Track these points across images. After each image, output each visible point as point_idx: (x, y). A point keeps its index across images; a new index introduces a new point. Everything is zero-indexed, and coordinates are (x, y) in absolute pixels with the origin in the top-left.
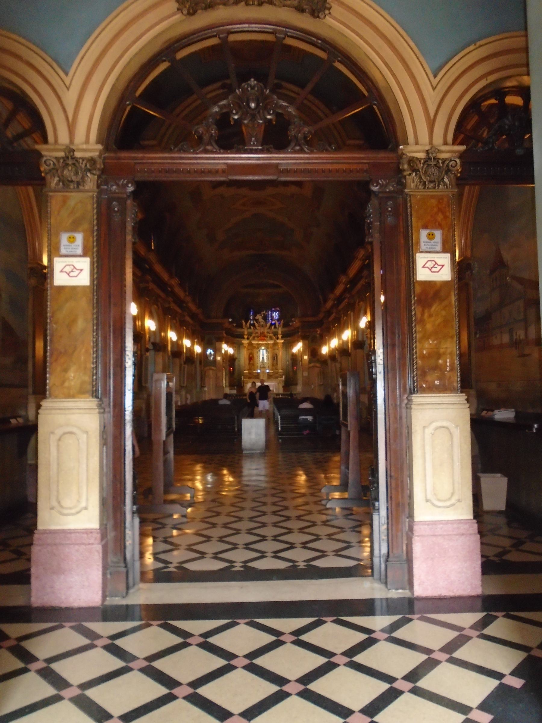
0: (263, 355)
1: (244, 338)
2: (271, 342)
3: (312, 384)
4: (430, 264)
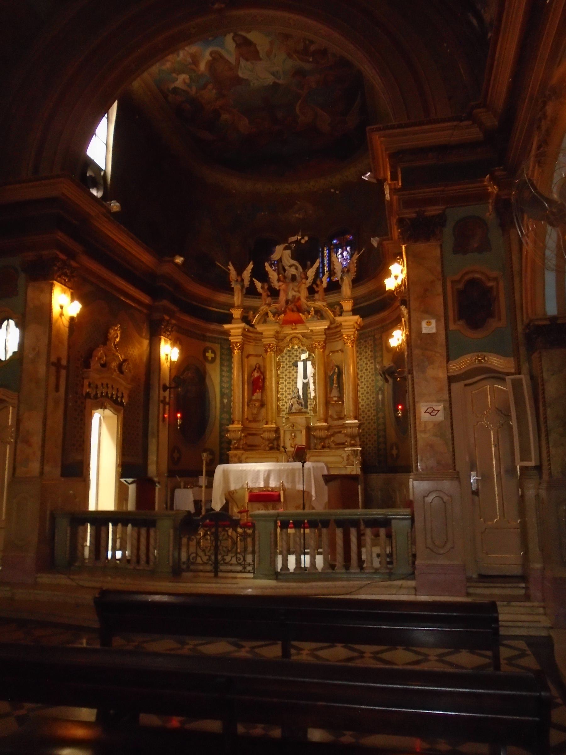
0: (305, 377)
2: (321, 326)
3: (473, 467)
4: (429, 410)
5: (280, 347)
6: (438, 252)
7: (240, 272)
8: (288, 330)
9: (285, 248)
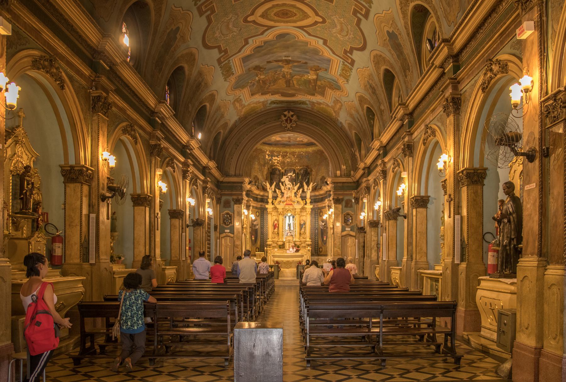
1: (267, 203)
6: (341, 207)
7: (271, 186)
8: (287, 207)
9: (287, 177)
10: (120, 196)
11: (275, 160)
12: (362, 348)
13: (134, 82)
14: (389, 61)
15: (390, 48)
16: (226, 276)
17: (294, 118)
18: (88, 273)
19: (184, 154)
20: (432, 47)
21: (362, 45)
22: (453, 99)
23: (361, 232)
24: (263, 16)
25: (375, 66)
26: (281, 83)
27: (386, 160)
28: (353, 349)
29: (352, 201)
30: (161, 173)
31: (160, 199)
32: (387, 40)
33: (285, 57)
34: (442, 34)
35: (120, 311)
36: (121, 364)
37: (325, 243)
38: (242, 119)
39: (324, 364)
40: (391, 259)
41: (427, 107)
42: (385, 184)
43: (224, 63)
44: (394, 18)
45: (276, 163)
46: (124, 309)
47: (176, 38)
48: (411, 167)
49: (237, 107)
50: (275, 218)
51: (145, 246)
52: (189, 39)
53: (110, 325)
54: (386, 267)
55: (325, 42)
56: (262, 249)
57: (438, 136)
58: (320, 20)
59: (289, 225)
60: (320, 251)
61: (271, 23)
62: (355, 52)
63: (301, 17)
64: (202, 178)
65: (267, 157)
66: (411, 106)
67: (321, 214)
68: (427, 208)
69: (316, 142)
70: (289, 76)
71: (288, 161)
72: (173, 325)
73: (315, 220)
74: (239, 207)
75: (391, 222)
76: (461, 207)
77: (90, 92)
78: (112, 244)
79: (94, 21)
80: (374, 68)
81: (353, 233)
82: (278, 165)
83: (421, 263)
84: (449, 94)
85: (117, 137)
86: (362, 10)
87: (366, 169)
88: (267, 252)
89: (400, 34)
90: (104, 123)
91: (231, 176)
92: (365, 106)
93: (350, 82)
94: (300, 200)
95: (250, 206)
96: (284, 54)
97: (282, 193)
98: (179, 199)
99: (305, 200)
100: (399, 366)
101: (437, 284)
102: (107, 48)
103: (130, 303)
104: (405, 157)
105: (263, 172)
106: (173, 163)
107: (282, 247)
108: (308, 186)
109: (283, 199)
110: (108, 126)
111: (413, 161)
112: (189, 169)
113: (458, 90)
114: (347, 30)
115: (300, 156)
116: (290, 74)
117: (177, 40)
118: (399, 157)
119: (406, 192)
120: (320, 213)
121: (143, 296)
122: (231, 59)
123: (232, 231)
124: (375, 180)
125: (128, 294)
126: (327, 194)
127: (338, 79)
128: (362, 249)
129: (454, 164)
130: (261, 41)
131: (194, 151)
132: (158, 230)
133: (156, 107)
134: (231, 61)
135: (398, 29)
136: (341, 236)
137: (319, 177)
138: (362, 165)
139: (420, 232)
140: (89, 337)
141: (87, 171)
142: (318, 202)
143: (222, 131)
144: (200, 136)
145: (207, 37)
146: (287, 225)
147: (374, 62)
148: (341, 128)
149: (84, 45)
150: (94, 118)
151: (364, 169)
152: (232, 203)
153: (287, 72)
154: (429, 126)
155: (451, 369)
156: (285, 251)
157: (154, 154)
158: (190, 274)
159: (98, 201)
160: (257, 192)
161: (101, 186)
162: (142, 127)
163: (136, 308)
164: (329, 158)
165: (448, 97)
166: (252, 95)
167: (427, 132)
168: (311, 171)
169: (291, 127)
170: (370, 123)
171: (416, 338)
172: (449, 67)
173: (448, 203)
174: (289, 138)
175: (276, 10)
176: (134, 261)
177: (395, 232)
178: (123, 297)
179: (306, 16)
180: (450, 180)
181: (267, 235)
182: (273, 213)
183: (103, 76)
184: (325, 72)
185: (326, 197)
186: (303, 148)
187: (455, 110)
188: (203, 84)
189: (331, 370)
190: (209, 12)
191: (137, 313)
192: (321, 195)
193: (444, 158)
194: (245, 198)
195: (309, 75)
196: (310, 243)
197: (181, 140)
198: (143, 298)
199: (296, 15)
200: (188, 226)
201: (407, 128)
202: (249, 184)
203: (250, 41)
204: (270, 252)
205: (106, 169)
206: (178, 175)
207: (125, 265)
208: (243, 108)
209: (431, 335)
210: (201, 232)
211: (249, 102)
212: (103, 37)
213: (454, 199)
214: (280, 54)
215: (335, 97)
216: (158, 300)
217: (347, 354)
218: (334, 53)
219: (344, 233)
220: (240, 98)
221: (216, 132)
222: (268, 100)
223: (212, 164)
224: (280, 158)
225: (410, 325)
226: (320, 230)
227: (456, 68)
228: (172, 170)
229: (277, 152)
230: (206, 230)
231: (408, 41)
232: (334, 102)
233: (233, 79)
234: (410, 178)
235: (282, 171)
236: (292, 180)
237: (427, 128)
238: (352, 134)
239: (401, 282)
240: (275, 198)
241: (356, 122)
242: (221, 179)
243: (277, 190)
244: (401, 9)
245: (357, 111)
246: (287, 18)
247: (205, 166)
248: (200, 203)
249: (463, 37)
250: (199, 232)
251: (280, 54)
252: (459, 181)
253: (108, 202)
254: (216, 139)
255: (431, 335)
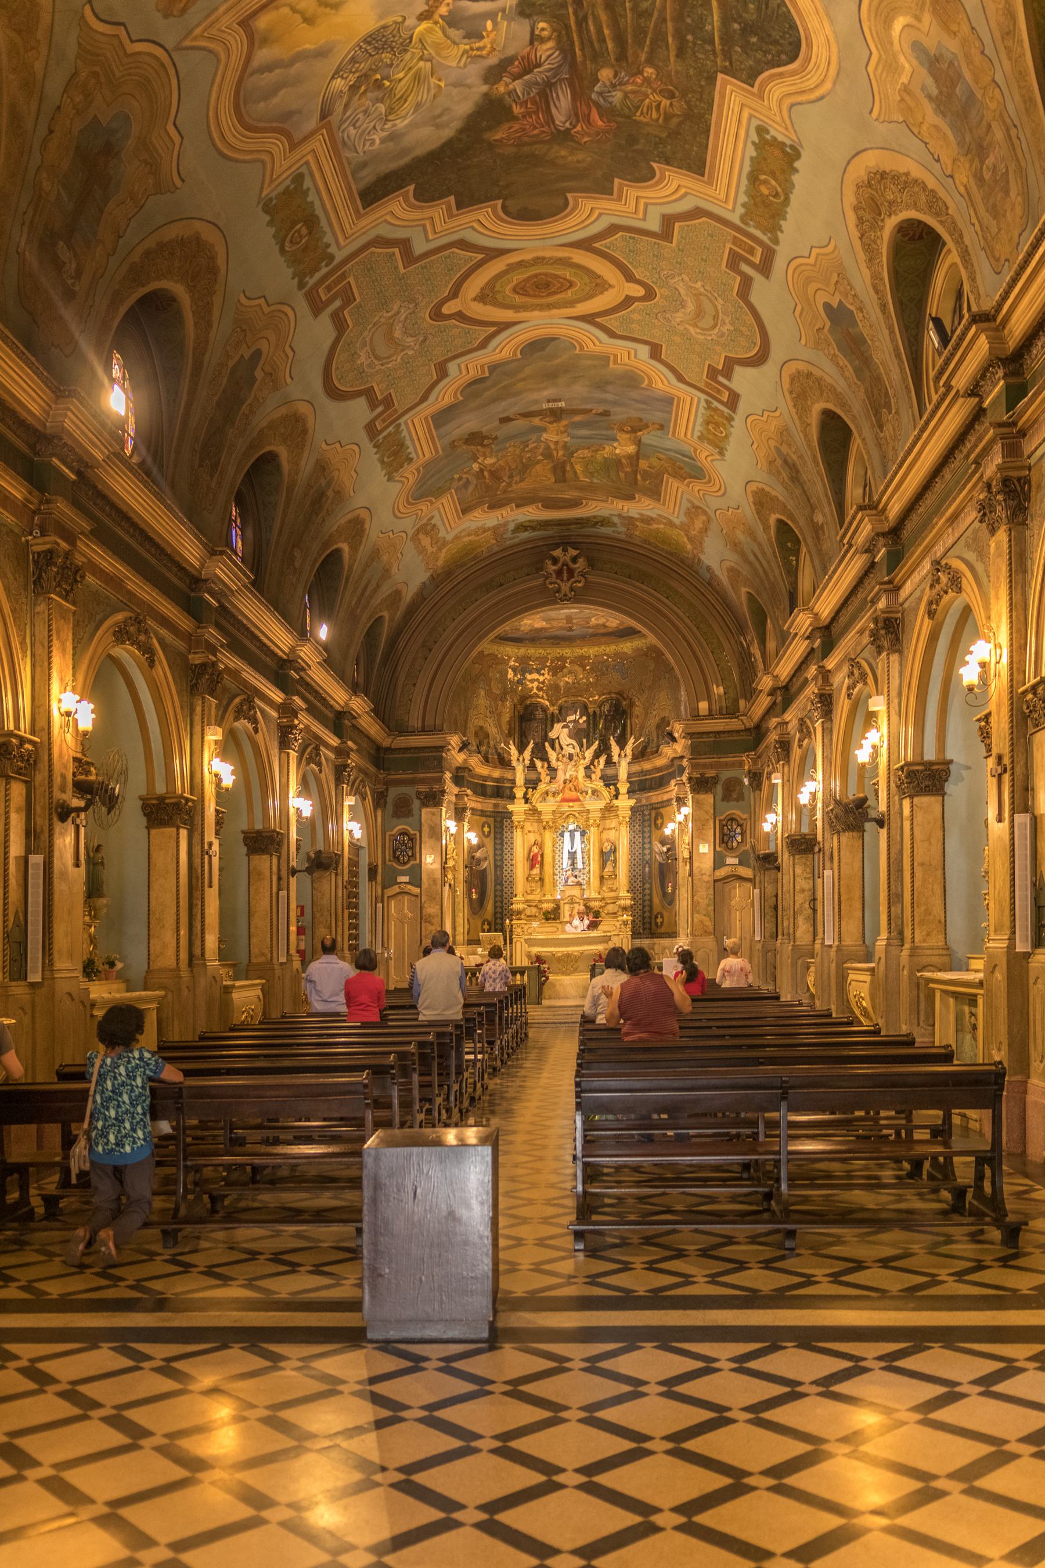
1: (512, 798)
5: (186, 660)
6: (711, 801)
7: (521, 751)
8: (565, 807)
10: (104, 804)
11: (532, 681)
12: (740, 1195)
13: (145, 508)
14: (833, 389)
15: (834, 349)
16: (386, 1002)
17: (581, 565)
18: (22, 1009)
19: (281, 682)
20: (945, 339)
21: (757, 349)
22: (1006, 481)
23: (768, 869)
24: (482, 298)
25: (795, 406)
26: (542, 474)
27: (830, 664)
28: (712, 1199)
29: (741, 782)
30: (219, 737)
31: (217, 804)
32: (826, 330)
33: (549, 401)
34: (978, 297)
35: (90, 1106)
36: (89, 1244)
37: (669, 900)
38: (440, 579)
39: (624, 1243)
40: (848, 941)
41: (937, 510)
42: (827, 731)
43: (385, 433)
44: (842, 264)
45: (535, 691)
46: (99, 1100)
47: (252, 380)
48: (895, 682)
49: (424, 548)
50: (532, 838)
51: (178, 931)
52: (288, 380)
53: (68, 1142)
54: (834, 965)
55: (656, 353)
56: (497, 924)
57: (969, 590)
58: (639, 291)
59: (572, 856)
60: (656, 924)
61: (507, 315)
62: (739, 371)
63: (587, 288)
64: (334, 741)
65: (510, 674)
66: (895, 509)
67: (659, 822)
68: (943, 794)
69: (638, 626)
70: (561, 453)
71: (567, 683)
72: (231, 1139)
73: (644, 838)
74: (433, 814)
75: (845, 837)
76: (1033, 789)
77: (27, 541)
78: (93, 929)
79: (33, 359)
80: (793, 411)
81: (746, 872)
82: (541, 693)
83: (929, 952)
84: (994, 468)
85: (100, 651)
86: (751, 251)
87: (779, 692)
88: (511, 931)
89: (861, 309)
90: (64, 618)
91: (412, 733)
92: (773, 518)
93: (728, 454)
94: (599, 785)
95: (464, 809)
96: (546, 393)
97: (552, 770)
98: (271, 802)
99: (615, 785)
100: (836, 1250)
101: (973, 1010)
102: (68, 424)
103: (113, 1085)
104: (879, 653)
105: (500, 715)
106: (252, 707)
107: (553, 915)
108: (622, 748)
109: (554, 787)
110: (76, 625)
111: (901, 665)
112: (296, 722)
113: (1022, 455)
114: (714, 313)
115: (600, 668)
116: (565, 446)
117: (257, 384)
118: (866, 654)
119: (884, 751)
120: (656, 819)
121: (148, 1065)
122: (402, 420)
123: (416, 880)
124: (802, 722)
125: (109, 1061)
126: (674, 769)
127: (695, 450)
128: (770, 912)
129: (1011, 669)
130: (482, 367)
131: (309, 672)
132: (210, 886)
133: (203, 566)
134: (403, 427)
135: (855, 296)
136: (711, 880)
137: (653, 722)
138: (766, 683)
139: (922, 864)
140: (16, 1176)
141: (21, 745)
142: (651, 789)
143: (386, 614)
144: (323, 633)
145: (337, 368)
146: (566, 855)
147: (791, 392)
148: (709, 584)
149: (10, 423)
150: (38, 609)
151: (771, 693)
152: (416, 803)
153: (557, 443)
154: (943, 562)
155: (988, 1260)
156: (559, 926)
157: (201, 689)
158: (300, 1000)
159: (50, 820)
160: (483, 770)
161: (57, 780)
162: (166, 619)
163: (130, 1097)
164: (676, 668)
165: (991, 479)
166: (465, 511)
167: (938, 581)
168: (632, 704)
169: (572, 590)
170: (787, 563)
171: (901, 1169)
172: (996, 391)
173: (995, 780)
174: (569, 619)
175: (517, 278)
176: (149, 971)
177: (857, 864)
178: (95, 1070)
179: (600, 285)
180: (999, 716)
181: (512, 884)
182: (528, 826)
183: (60, 499)
184: (659, 433)
185: (672, 776)
186: (606, 644)
187: (1014, 514)
188: (330, 493)
189: (638, 1261)
190: (338, 303)
191: (132, 1110)
192: (659, 769)
193: (980, 651)
194: (451, 789)
195: (615, 444)
196: (628, 902)
197: (273, 647)
198: (148, 1072)
199: (571, 284)
200: (294, 872)
201: (885, 571)
202: (461, 750)
203: (452, 367)
204: (519, 930)
205: (69, 737)
206: (268, 740)
207: (127, 981)
208: (440, 549)
209: (941, 1159)
210: (331, 886)
211: (455, 532)
212: (58, 397)
213: (1013, 768)
214: (535, 396)
215: (689, 501)
216: (187, 1073)
217: (693, 1215)
218: (681, 379)
219: (722, 873)
220: (433, 522)
221: (370, 618)
222: (508, 522)
223: (359, 705)
224: (546, 676)
225: (885, 1132)
226: (656, 867)
227: (1015, 393)
228: (250, 726)
229: (537, 659)
230: (346, 878)
231: (883, 326)
232: (688, 513)
233: (410, 474)
234: (892, 712)
235: (551, 709)
236: (580, 735)
237: (938, 570)
238: (739, 598)
239: (873, 1007)
240: (532, 784)
241: (751, 564)
242: (387, 742)
243: (539, 764)
244: (861, 238)
245: (752, 534)
246: (548, 295)
247: (339, 709)
248: (328, 811)
249: (1032, 302)
250: (328, 886)
251: (535, 396)
252: (1025, 718)
253: (78, 821)
254: (371, 635)
255: (941, 1159)
